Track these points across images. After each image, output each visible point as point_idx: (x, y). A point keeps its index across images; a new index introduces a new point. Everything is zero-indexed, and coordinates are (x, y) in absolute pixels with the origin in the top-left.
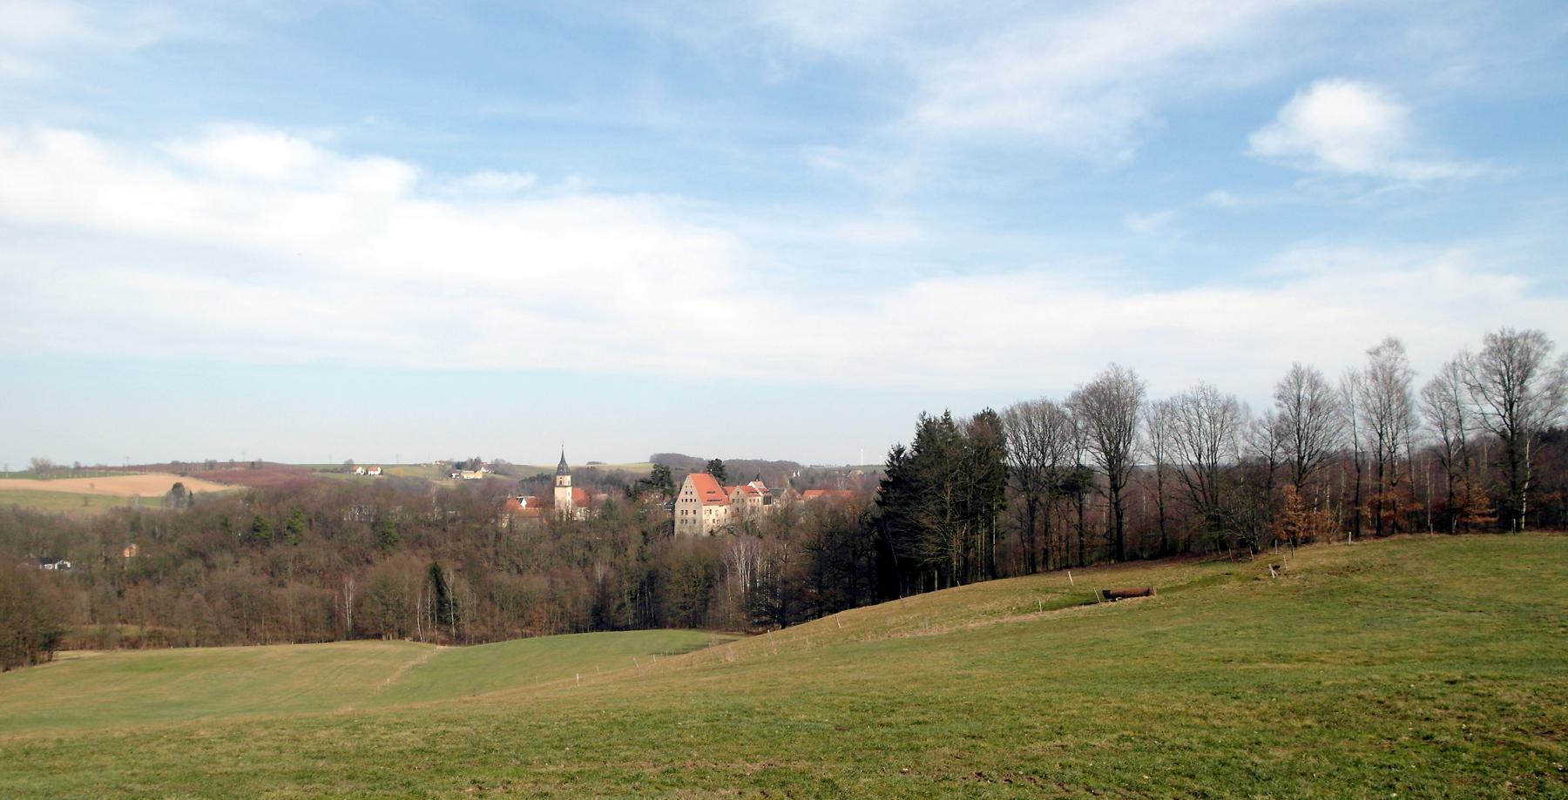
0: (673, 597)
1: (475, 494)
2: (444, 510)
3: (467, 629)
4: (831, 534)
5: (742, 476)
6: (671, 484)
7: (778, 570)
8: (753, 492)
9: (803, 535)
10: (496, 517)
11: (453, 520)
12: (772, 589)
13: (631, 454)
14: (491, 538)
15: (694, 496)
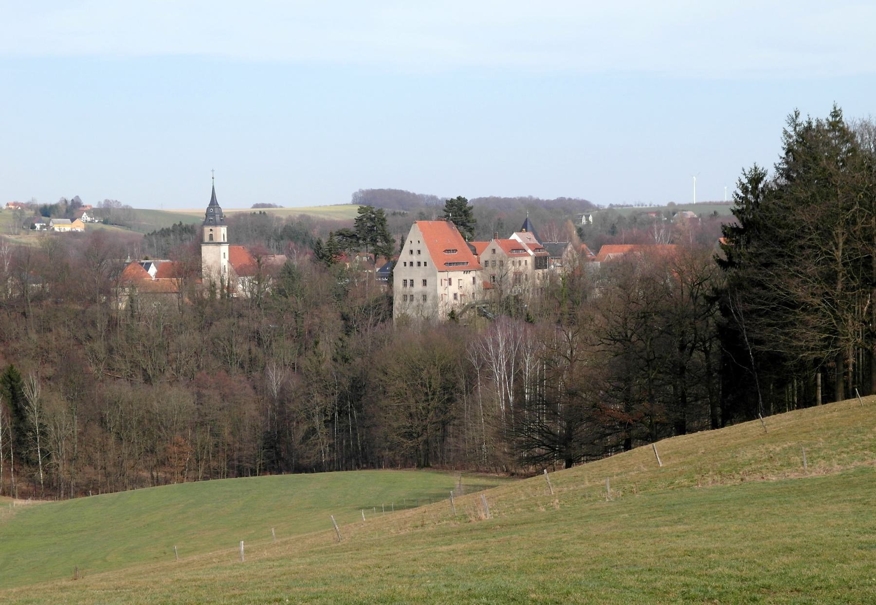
0: (390, 420)
1: (73, 255)
2: (23, 283)
3: (63, 471)
4: (645, 316)
5: (500, 224)
6: (386, 239)
7: (559, 373)
8: (517, 249)
9: (598, 316)
10: (108, 293)
11: (38, 298)
12: (550, 403)
13: (320, 189)
14: (101, 326)
15: (423, 258)
